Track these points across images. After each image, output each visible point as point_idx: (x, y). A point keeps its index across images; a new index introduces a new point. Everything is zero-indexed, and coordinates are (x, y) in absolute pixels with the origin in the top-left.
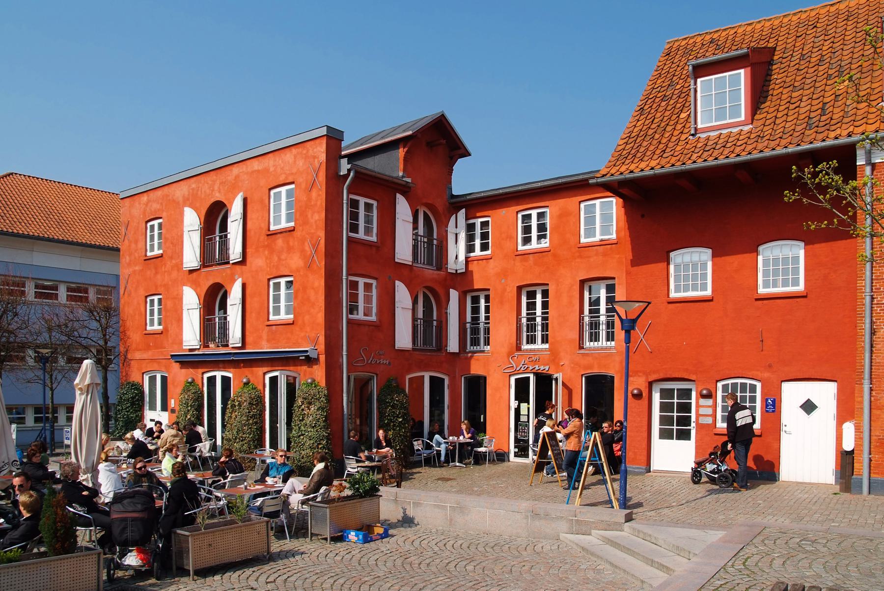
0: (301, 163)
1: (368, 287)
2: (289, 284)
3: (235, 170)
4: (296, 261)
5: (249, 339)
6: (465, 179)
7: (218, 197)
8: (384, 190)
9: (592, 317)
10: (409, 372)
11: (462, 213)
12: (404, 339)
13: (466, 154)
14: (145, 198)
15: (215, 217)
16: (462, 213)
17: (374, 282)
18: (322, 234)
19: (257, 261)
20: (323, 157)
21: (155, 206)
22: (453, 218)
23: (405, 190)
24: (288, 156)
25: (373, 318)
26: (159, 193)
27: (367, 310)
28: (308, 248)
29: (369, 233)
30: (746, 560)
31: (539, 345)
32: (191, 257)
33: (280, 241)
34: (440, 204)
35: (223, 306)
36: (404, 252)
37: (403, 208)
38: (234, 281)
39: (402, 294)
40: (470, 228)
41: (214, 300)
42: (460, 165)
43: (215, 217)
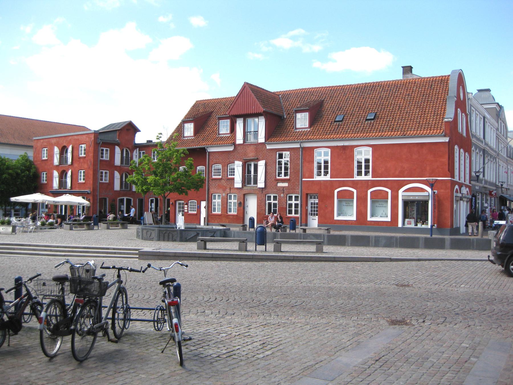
0: (87, 139)
1: (106, 173)
2: (84, 172)
3: (70, 138)
4: (86, 166)
5: (73, 187)
6: (140, 139)
7: (65, 144)
8: (111, 145)
9: (61, 206)
10: (119, 197)
11: (138, 149)
12: (117, 187)
13: (139, 131)
14: (42, 141)
15: (63, 150)
16: (138, 149)
17: (108, 172)
18: (92, 159)
19: (76, 165)
20: (93, 139)
21: (45, 144)
22: (135, 151)
23: (118, 145)
24: (84, 137)
25: (108, 182)
26: (47, 140)
27: (105, 180)
28: (89, 162)
29: (106, 157)
30: (444, 322)
31: (20, 213)
32: (56, 162)
33: (82, 160)
34: (130, 147)
35: (67, 152)
36: (118, 162)
37: (118, 150)
38: (69, 170)
39: (117, 175)
40: (140, 153)
41: (63, 175)
42: (138, 135)
43: (63, 150)
